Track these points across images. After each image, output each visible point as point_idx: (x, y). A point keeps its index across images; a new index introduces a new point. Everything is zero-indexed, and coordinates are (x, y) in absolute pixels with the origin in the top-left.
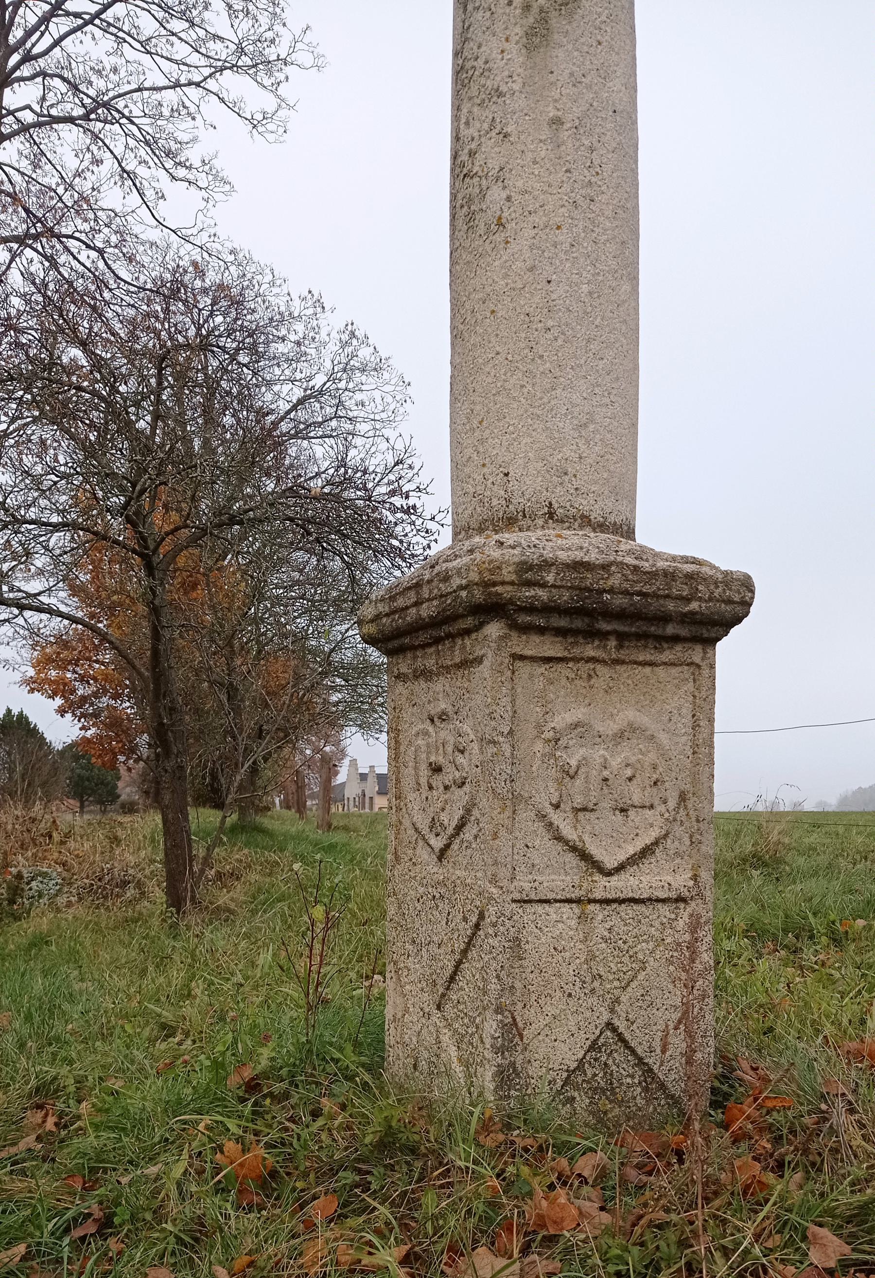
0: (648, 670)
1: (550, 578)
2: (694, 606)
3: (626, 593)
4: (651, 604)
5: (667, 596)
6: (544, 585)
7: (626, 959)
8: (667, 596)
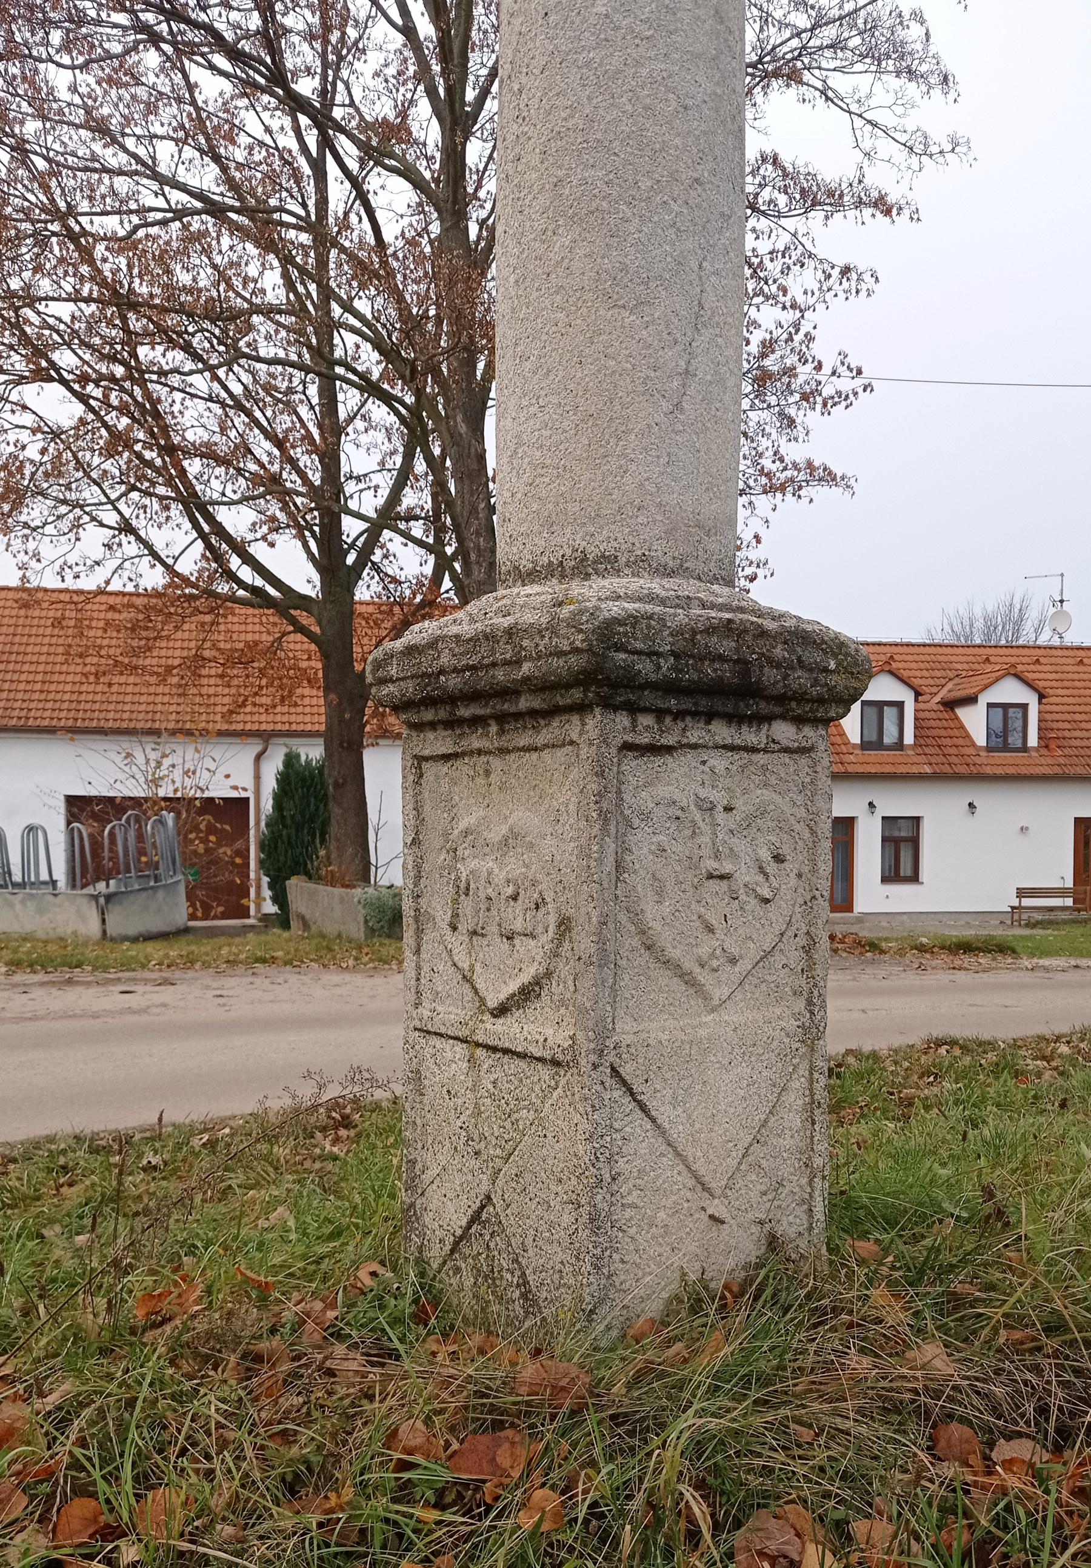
0: (535, 756)
1: (394, 671)
2: (526, 668)
3: (456, 670)
4: (481, 678)
5: (494, 665)
6: (391, 680)
7: (508, 1124)
8: (494, 665)
